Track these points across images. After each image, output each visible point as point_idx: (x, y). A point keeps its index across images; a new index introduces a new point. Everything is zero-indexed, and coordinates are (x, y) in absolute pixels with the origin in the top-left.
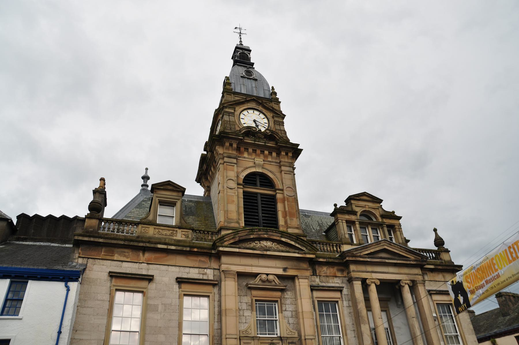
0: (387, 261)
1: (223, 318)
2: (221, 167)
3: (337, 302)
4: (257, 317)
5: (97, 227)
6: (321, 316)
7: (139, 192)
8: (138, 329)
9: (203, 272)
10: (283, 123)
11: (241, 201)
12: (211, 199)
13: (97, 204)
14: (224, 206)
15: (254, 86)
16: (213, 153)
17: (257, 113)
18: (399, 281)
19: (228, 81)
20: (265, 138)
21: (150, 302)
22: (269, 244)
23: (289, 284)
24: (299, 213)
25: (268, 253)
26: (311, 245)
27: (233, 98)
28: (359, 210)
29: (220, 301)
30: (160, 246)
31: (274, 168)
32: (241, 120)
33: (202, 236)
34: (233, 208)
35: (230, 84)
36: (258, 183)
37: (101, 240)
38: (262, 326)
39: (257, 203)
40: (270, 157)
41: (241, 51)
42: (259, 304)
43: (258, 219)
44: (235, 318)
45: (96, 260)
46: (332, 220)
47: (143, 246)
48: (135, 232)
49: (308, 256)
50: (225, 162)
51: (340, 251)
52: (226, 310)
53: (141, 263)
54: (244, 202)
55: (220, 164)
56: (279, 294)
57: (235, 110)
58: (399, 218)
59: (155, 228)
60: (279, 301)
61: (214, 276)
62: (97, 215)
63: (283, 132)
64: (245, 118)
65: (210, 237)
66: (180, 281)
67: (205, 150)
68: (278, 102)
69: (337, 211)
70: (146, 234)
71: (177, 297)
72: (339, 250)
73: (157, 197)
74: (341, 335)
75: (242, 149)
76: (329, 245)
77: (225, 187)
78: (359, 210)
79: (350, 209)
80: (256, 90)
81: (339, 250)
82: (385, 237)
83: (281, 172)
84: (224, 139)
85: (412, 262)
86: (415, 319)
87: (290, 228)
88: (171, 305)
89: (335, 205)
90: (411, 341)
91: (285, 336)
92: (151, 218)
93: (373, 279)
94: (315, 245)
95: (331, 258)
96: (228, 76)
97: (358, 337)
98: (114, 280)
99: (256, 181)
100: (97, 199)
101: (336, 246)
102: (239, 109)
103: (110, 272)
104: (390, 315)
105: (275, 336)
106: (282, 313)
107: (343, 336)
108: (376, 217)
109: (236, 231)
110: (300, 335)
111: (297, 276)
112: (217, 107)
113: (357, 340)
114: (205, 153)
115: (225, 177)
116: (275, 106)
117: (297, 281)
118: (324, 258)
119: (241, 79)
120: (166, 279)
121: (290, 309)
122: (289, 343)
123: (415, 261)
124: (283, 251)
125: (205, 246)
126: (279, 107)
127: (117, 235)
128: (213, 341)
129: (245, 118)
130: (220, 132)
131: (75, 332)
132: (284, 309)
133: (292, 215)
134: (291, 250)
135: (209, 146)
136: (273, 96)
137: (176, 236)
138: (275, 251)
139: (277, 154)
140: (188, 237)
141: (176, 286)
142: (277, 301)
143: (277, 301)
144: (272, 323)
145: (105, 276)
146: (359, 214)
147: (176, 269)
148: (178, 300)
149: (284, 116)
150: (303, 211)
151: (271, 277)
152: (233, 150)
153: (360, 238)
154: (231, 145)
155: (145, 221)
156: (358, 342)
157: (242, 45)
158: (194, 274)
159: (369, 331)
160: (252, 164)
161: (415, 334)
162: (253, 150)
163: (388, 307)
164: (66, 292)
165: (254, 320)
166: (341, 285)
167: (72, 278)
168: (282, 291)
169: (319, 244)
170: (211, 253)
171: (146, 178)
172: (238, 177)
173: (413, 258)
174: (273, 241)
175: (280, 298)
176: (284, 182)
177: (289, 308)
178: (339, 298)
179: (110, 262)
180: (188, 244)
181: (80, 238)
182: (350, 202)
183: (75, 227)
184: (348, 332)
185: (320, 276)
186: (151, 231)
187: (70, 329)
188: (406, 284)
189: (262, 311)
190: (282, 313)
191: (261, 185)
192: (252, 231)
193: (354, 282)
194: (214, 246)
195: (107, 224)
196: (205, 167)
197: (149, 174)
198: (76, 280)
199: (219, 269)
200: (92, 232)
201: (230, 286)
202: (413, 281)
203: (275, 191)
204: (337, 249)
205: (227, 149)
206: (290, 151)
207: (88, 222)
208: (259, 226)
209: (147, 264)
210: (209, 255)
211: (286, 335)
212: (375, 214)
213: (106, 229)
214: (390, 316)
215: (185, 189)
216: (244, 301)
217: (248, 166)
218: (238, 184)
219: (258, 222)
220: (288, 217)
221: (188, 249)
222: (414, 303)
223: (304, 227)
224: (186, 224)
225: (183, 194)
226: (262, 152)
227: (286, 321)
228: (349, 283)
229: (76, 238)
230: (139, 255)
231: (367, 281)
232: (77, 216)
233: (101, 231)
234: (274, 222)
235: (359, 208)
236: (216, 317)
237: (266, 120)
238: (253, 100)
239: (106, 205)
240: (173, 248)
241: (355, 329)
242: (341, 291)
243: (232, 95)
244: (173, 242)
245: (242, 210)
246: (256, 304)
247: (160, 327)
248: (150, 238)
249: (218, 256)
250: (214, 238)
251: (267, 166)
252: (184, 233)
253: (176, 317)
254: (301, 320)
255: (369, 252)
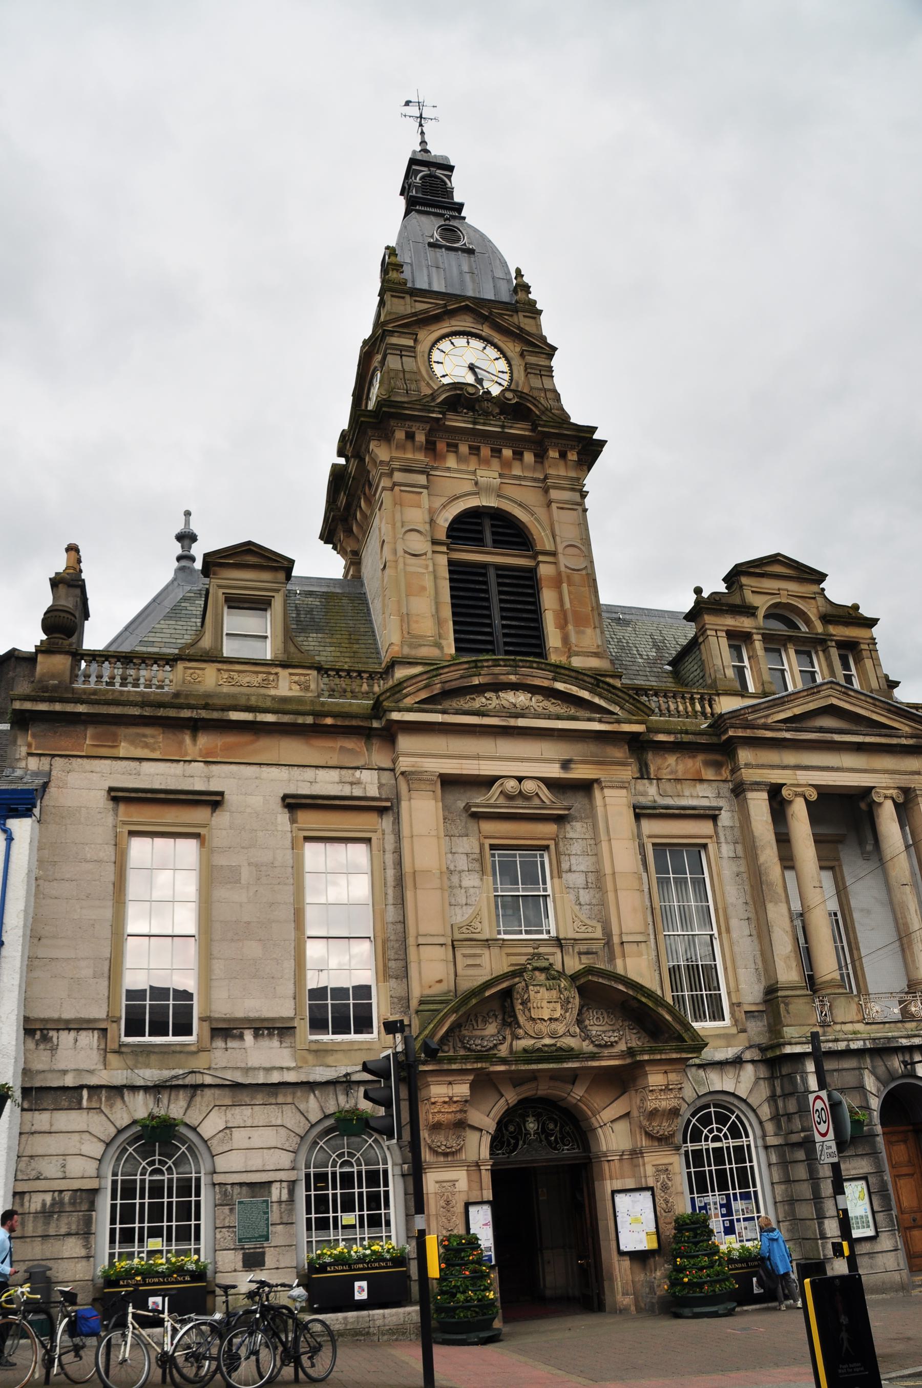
0: (837, 738)
1: (409, 895)
2: (386, 496)
3: (705, 846)
4: (496, 890)
5: (68, 673)
6: (663, 883)
7: (170, 576)
8: (192, 929)
9: (351, 779)
10: (550, 369)
11: (445, 586)
12: (362, 585)
13: (63, 614)
14: (399, 602)
15: (466, 268)
16: (362, 460)
17: (476, 344)
18: (867, 791)
19: (393, 259)
20: (501, 413)
21: (220, 860)
22: (521, 699)
23: (577, 802)
24: (600, 615)
25: (521, 722)
26: (634, 698)
27: (408, 310)
28: (762, 603)
29: (398, 851)
30: (235, 716)
31: (531, 496)
32: (435, 366)
33: (343, 683)
34: (422, 606)
35: (398, 267)
36: (488, 537)
37: (81, 708)
38: (510, 912)
39: (486, 591)
40: (517, 464)
41: (425, 171)
42: (499, 856)
43: (490, 634)
44: (439, 892)
45: (73, 760)
46: (690, 630)
47: (190, 719)
48: (167, 682)
49: (626, 728)
50: (395, 484)
51: (712, 714)
52: (414, 873)
53: (190, 761)
54: (452, 588)
55: (384, 489)
56: (550, 829)
57: (416, 340)
58: (871, 623)
59: (219, 670)
60: (552, 847)
61: (381, 786)
62: (66, 642)
63: (549, 395)
64: (447, 360)
65: (365, 687)
66: (294, 804)
67: (340, 454)
68: (534, 312)
69: (704, 607)
70: (197, 687)
71: (288, 843)
72: (708, 710)
73: (220, 587)
74: (715, 932)
75: (441, 446)
76: (683, 698)
77: (400, 552)
78: (762, 603)
79: (738, 601)
80: (473, 281)
81: (708, 710)
82: (832, 672)
83: (549, 503)
84: (391, 418)
85: (904, 741)
86: (908, 888)
87: (577, 654)
88: (272, 865)
89: (698, 591)
90: (897, 944)
91: (569, 936)
92: (206, 642)
93: (798, 785)
94: (644, 699)
95: (687, 732)
96: (393, 244)
97: (760, 937)
98: (122, 808)
99: (481, 532)
100: (62, 602)
101: (702, 700)
102: (426, 336)
103: (111, 789)
104: (843, 878)
105: (545, 936)
106: (560, 877)
107: (720, 933)
108: (808, 622)
109: (434, 668)
110: (608, 934)
111: (597, 781)
112: (367, 332)
113: (756, 942)
114: (342, 461)
115: (399, 524)
116: (527, 324)
117: (597, 793)
118: (669, 732)
119: (430, 252)
120: (256, 801)
121: (583, 868)
122: (580, 953)
123: (912, 737)
124: (558, 718)
125: (355, 710)
126: (539, 326)
127: (121, 692)
128: (384, 954)
129: (447, 360)
130: (380, 404)
131: (36, 941)
132: (565, 866)
133: (581, 621)
134: (581, 713)
135: (352, 442)
136: (521, 295)
137: (276, 688)
138: (538, 716)
139: (536, 456)
140: (307, 689)
141: (283, 817)
142: (547, 848)
143: (547, 848)
144: (536, 902)
145: (99, 798)
146: (761, 613)
147: (283, 773)
148: (289, 852)
149: (551, 351)
150: (611, 609)
151: (529, 786)
152: (416, 449)
153: (766, 677)
154: (410, 436)
155: (191, 651)
156: (758, 948)
157: (426, 151)
158: (327, 783)
159: (787, 920)
160: (468, 487)
161: (906, 925)
162: (470, 447)
163: (838, 859)
164: (4, 843)
165: (488, 897)
166: (714, 803)
167: (16, 810)
168: (560, 820)
169: (656, 695)
170: (371, 729)
171: (186, 538)
172: (432, 522)
173: (907, 729)
174: (533, 690)
175: (555, 839)
176: (557, 532)
177: (579, 864)
178: (711, 837)
179: (108, 762)
180: (308, 708)
181: (28, 706)
182: (738, 581)
183: (13, 679)
184: (734, 923)
185: (658, 779)
186: (209, 678)
187: (24, 935)
188: (886, 797)
189: (507, 872)
190: (560, 877)
191: (497, 543)
192: (476, 667)
193: (750, 795)
194: (378, 710)
195: (94, 665)
196: (342, 499)
197: (195, 527)
198: (27, 813)
199: (393, 770)
200: (55, 688)
201: (423, 812)
202: (906, 791)
203: (534, 557)
204: (703, 707)
205: (401, 447)
206: (572, 448)
207: (44, 664)
208: (493, 652)
209: (206, 762)
210: (366, 734)
211: (571, 935)
212: (804, 613)
213: (93, 679)
214: (844, 883)
215: (292, 562)
216: (461, 850)
217: (458, 492)
218: (435, 542)
219: (491, 642)
220: (570, 627)
221: (309, 720)
222: (907, 847)
223: (613, 649)
224: (299, 655)
225: (289, 576)
226: (497, 452)
227: (572, 897)
228: (737, 796)
229: (17, 705)
230: (181, 743)
231: (785, 792)
232: (14, 650)
233: (79, 685)
234: (534, 641)
235: (761, 596)
236: (390, 891)
237: (502, 365)
238: (466, 310)
239: (86, 616)
240: (270, 718)
241: (752, 915)
242: (714, 818)
243: (408, 297)
244: (268, 704)
245: (447, 612)
246: (493, 856)
247: (249, 923)
248: (208, 695)
249: (389, 735)
250: (376, 689)
251: (510, 491)
252: (296, 678)
253: (286, 894)
254: (611, 895)
255: (788, 714)
